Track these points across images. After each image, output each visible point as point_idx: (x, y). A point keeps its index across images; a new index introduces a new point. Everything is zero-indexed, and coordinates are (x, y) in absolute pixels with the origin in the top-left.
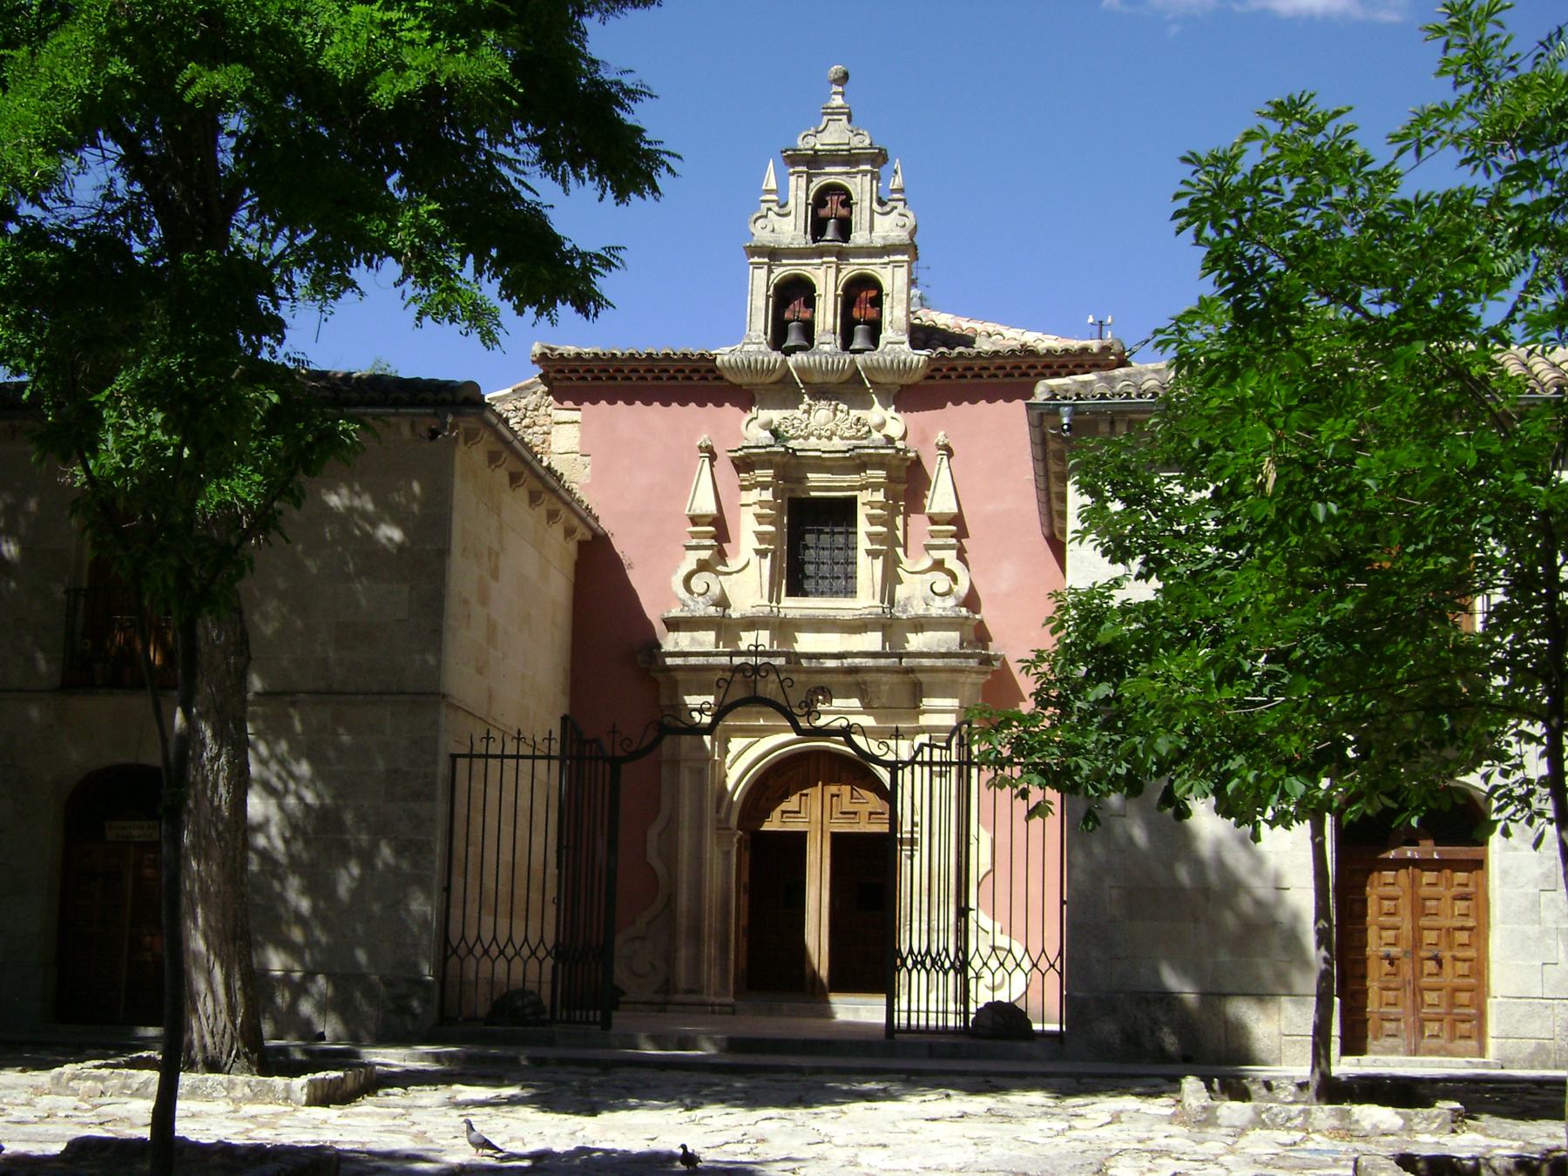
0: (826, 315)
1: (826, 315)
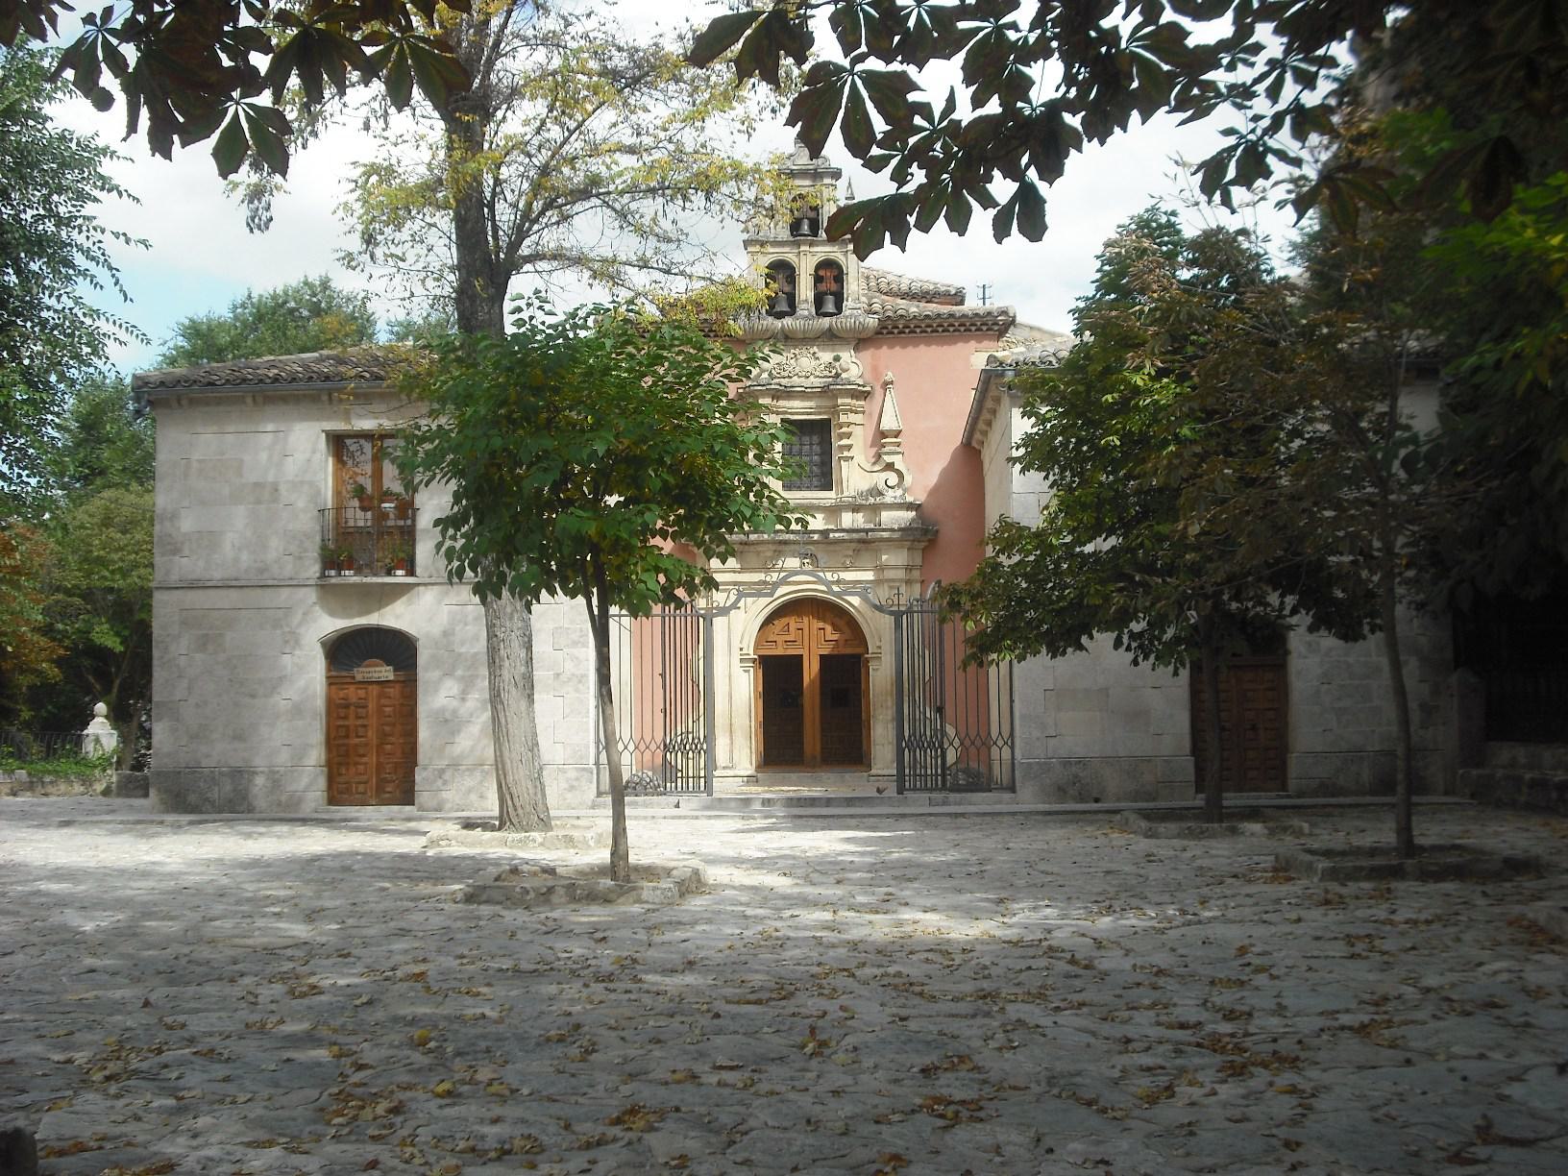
0: (805, 290)
1: (805, 290)
